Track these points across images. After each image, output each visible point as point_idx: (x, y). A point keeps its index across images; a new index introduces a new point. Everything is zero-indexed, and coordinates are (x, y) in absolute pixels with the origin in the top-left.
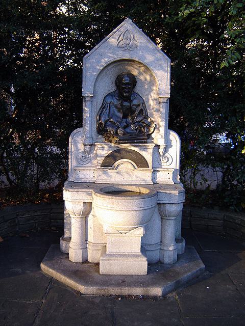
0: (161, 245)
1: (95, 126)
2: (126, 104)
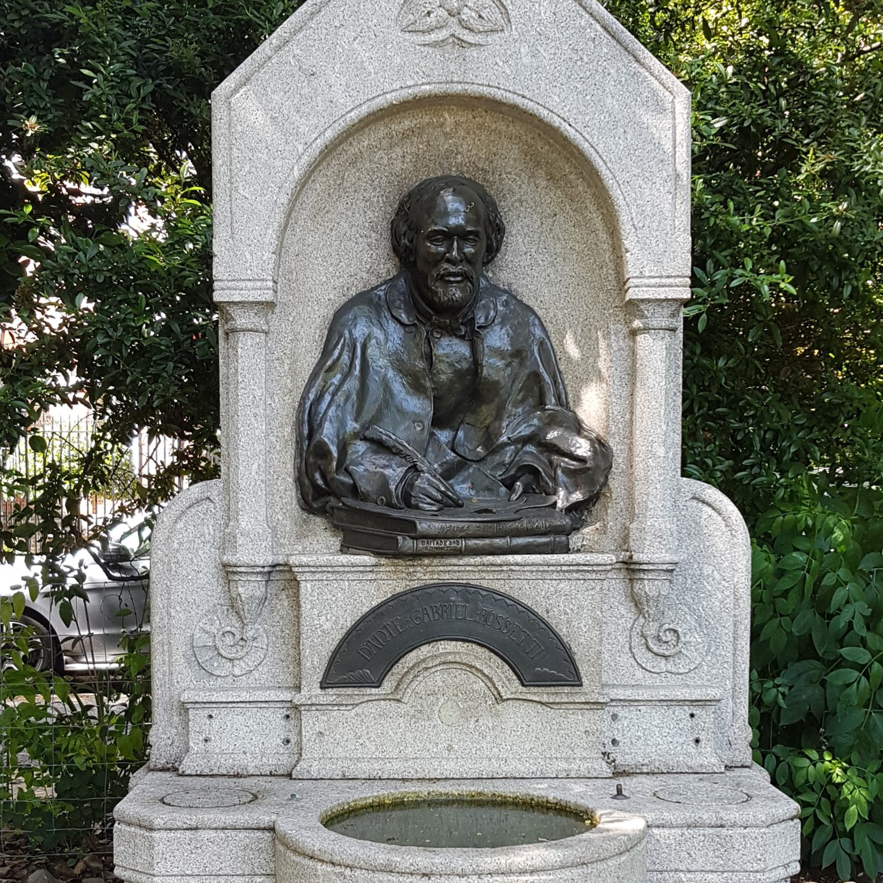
2: (451, 349)
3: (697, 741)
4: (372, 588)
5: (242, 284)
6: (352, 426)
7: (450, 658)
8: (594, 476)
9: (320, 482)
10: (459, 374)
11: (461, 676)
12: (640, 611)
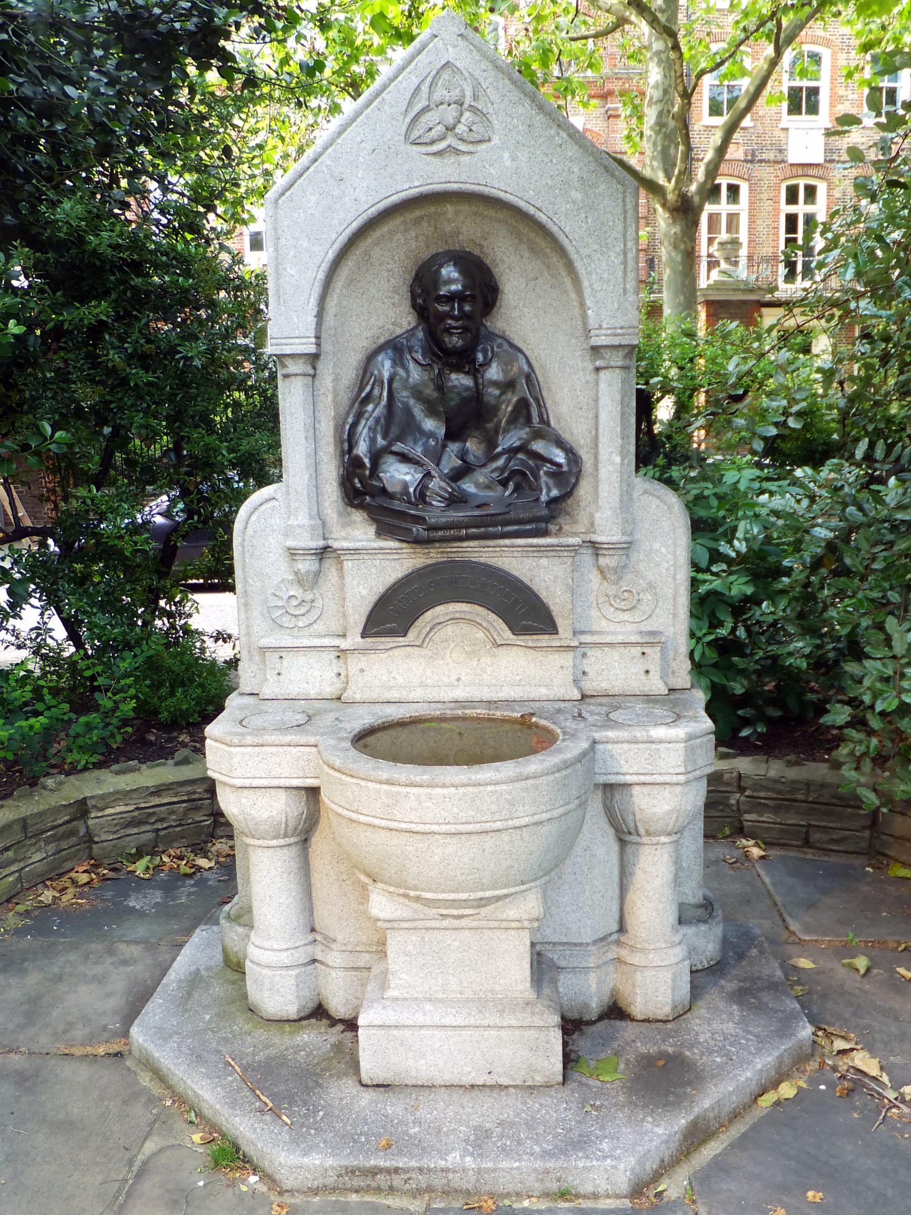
0: (618, 943)
1: (331, 471)
2: (460, 380)
3: (647, 672)
4: (396, 565)
5: (292, 341)
6: (381, 442)
7: (457, 615)
8: (569, 477)
9: (359, 485)
10: (465, 401)
11: (464, 628)
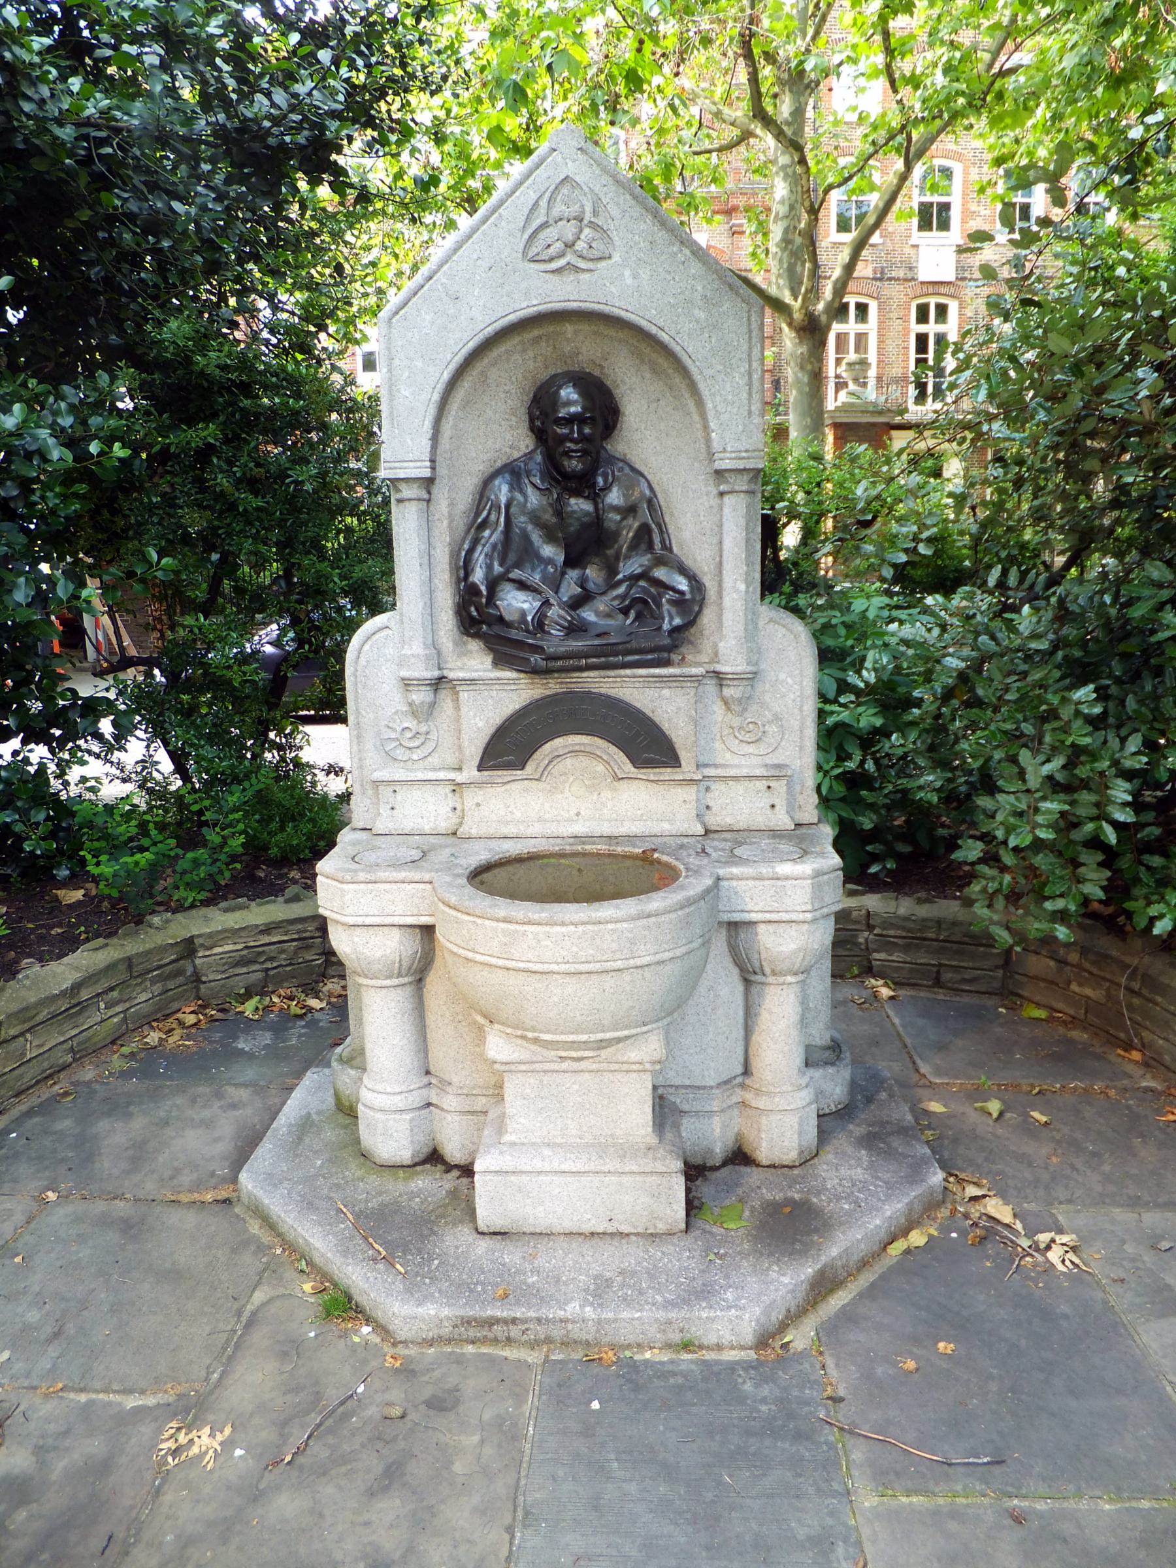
0: (743, 1086)
1: (446, 599)
2: (579, 505)
4: (514, 695)
8: (691, 606)
10: (585, 527)
11: (584, 761)
12: (729, 709)
